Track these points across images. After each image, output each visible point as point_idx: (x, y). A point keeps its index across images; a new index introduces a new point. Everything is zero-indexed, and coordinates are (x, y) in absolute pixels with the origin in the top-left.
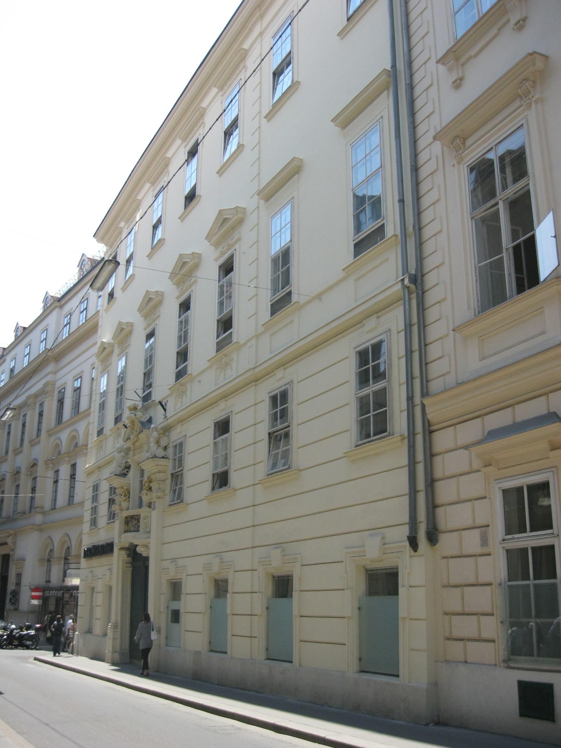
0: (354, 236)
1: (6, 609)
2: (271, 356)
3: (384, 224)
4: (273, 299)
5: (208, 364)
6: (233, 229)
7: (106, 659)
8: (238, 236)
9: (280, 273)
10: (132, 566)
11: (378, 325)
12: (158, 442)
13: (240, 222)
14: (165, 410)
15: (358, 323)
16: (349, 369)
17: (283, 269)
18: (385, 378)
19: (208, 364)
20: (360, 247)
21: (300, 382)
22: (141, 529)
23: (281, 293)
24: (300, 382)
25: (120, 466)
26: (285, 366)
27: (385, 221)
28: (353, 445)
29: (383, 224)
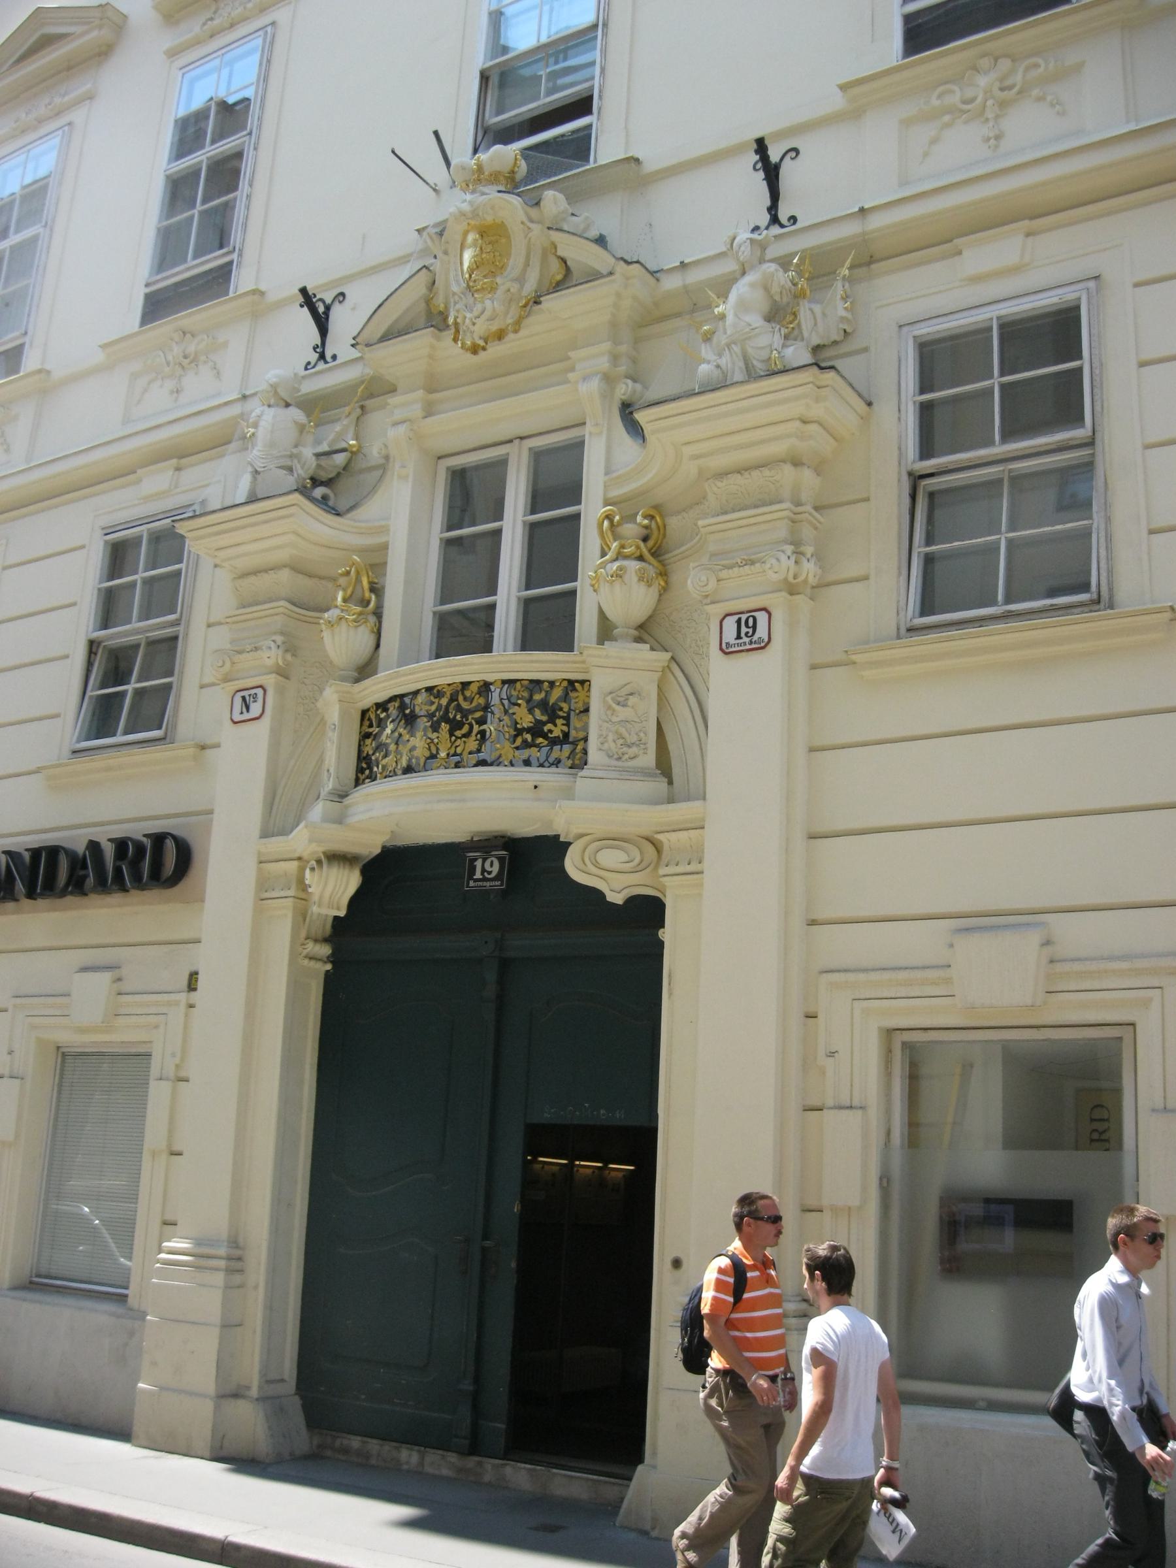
0: (151, 275)
1: (147, 1146)
2: (121, 434)
3: (231, 263)
4: (157, 281)
5: (100, 357)
6: (69, 68)
7: (138, 1429)
8: (89, 86)
9: (196, 212)
10: (334, 959)
11: (176, 487)
12: (779, 314)
13: (99, 55)
14: (323, 330)
15: (123, 473)
16: (83, 577)
17: (25, 283)
18: (1083, 426)
19: (100, 357)
20: (157, 305)
21: (11, 567)
22: (594, 755)
23: (194, 266)
24: (11, 567)
25: (290, 469)
26: (184, 461)
27: (235, 256)
28: (66, 752)
29: (22, 346)
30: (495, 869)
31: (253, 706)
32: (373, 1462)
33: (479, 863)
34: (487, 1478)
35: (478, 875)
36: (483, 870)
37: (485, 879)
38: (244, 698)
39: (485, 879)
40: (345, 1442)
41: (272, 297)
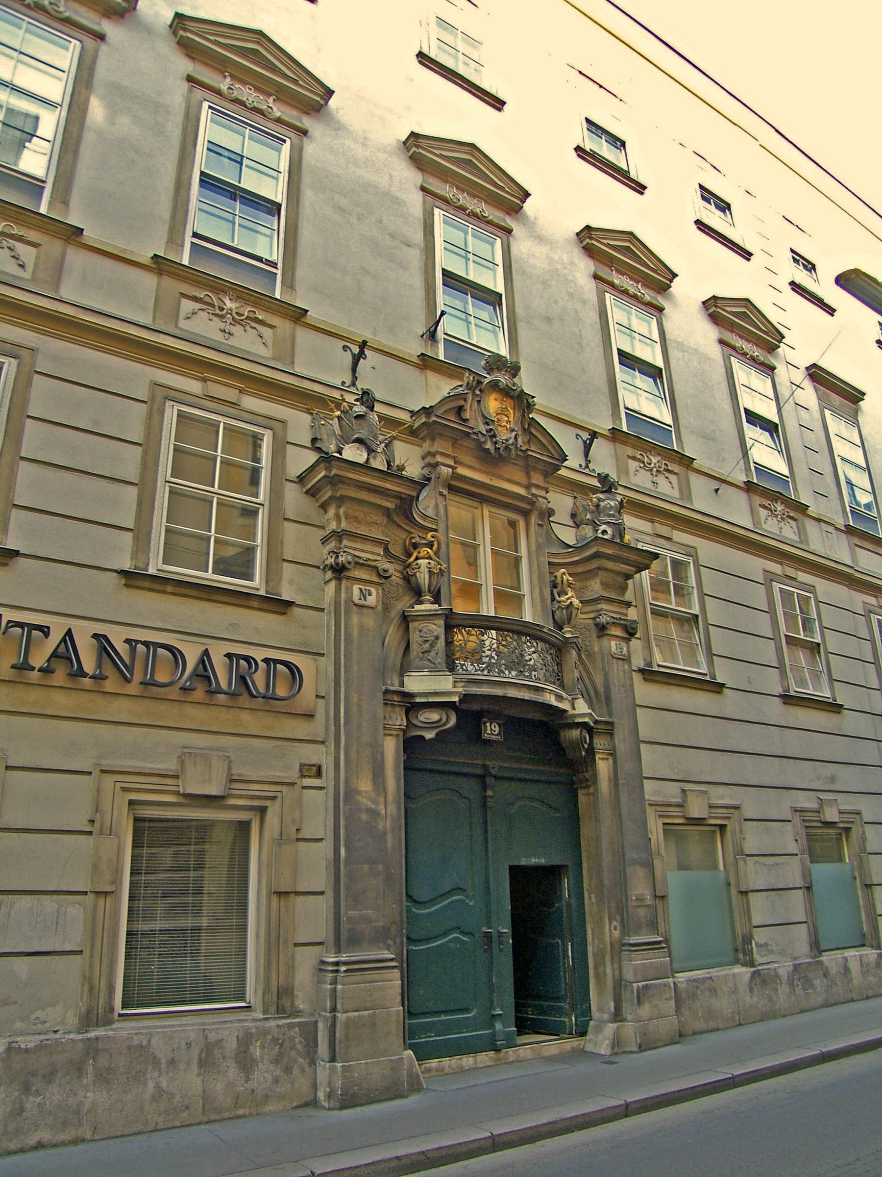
30: (497, 729)
31: (368, 598)
32: (446, 1071)
33: (488, 724)
34: (511, 1059)
35: (489, 731)
36: (491, 729)
37: (492, 734)
38: (361, 589)
39: (492, 734)
40: (427, 1065)
41: (308, 320)
